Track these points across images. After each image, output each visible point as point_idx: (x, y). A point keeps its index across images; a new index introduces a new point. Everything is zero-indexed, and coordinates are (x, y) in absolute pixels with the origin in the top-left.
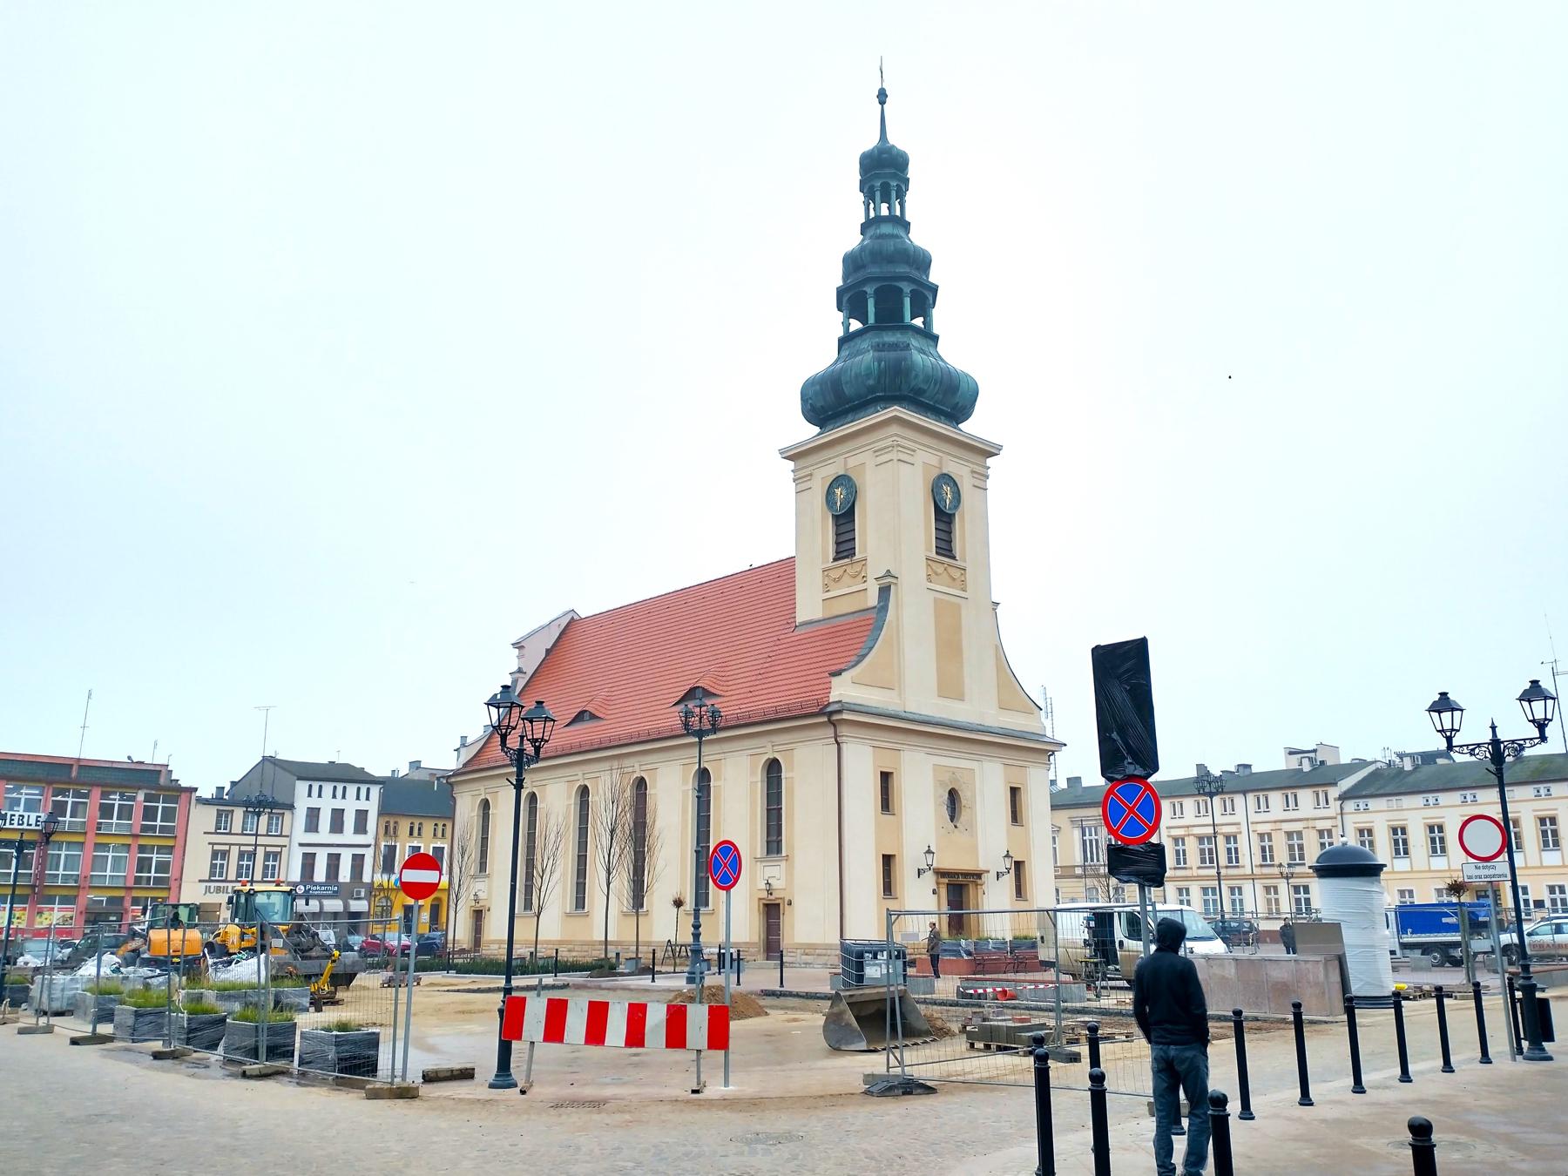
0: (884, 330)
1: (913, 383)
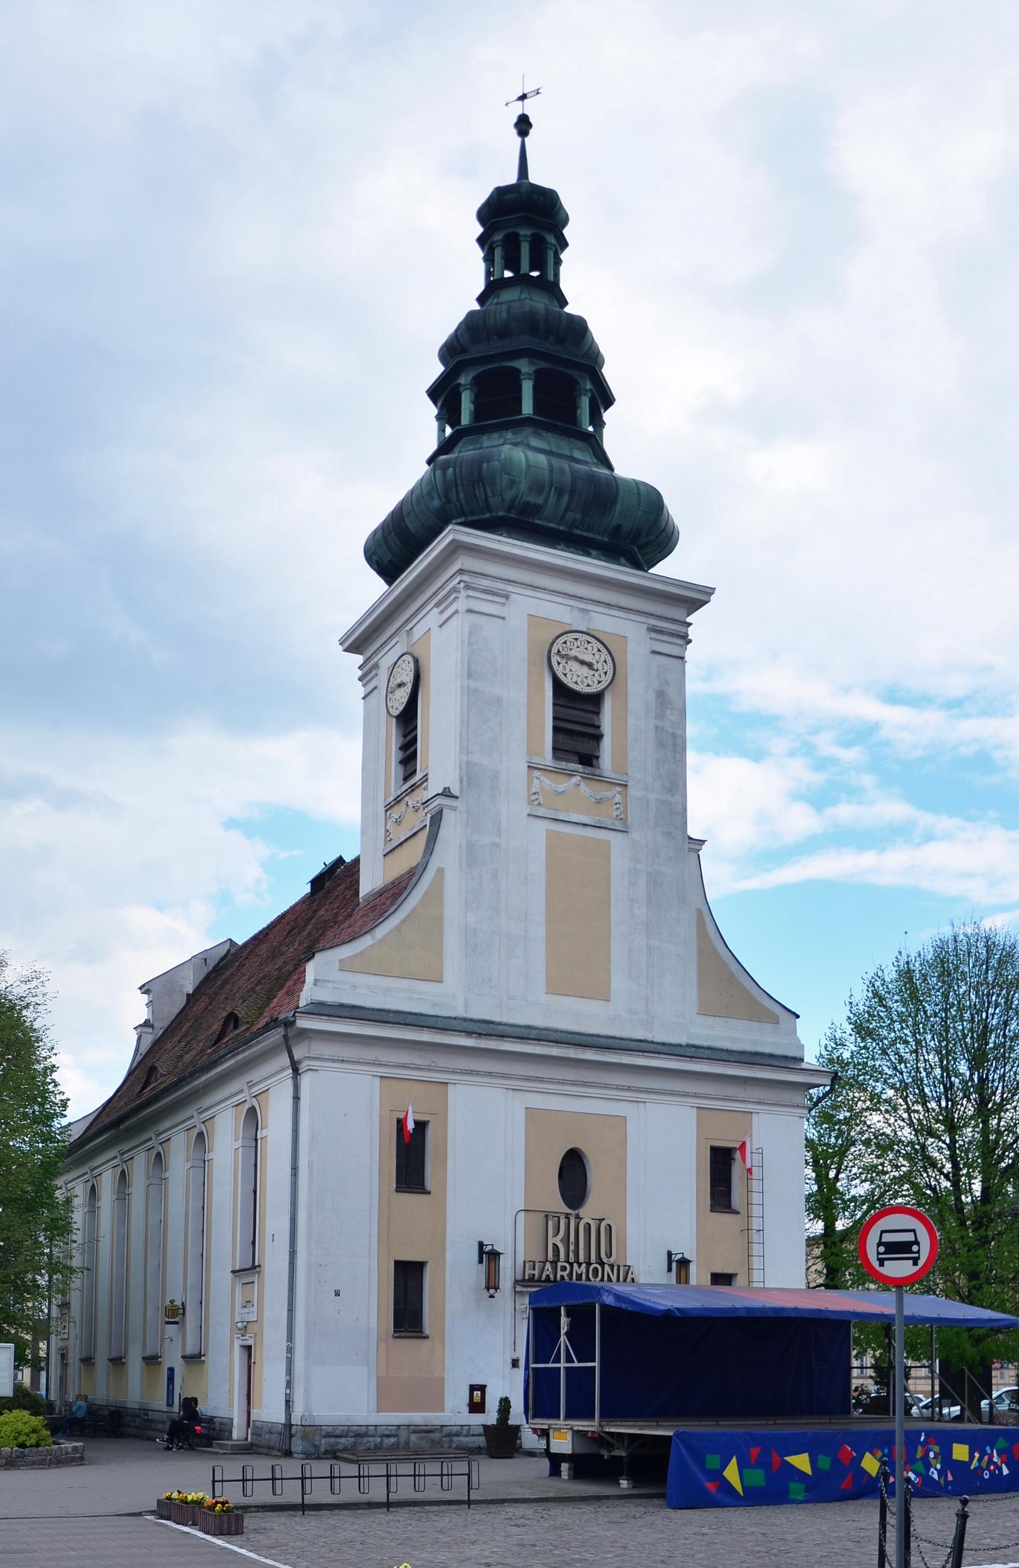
0: (484, 434)
1: (509, 495)
